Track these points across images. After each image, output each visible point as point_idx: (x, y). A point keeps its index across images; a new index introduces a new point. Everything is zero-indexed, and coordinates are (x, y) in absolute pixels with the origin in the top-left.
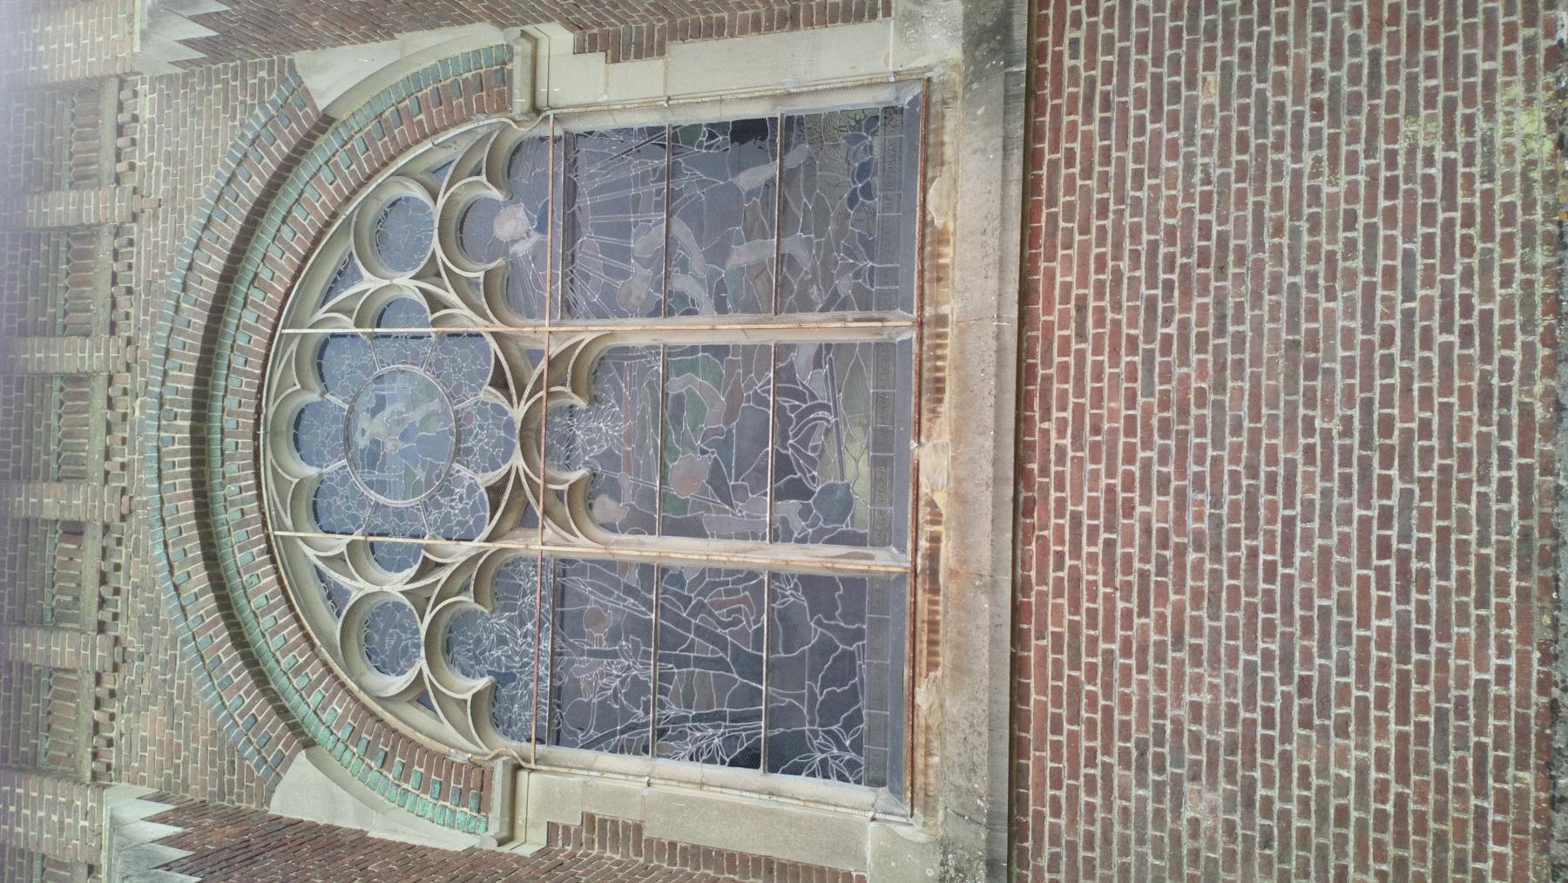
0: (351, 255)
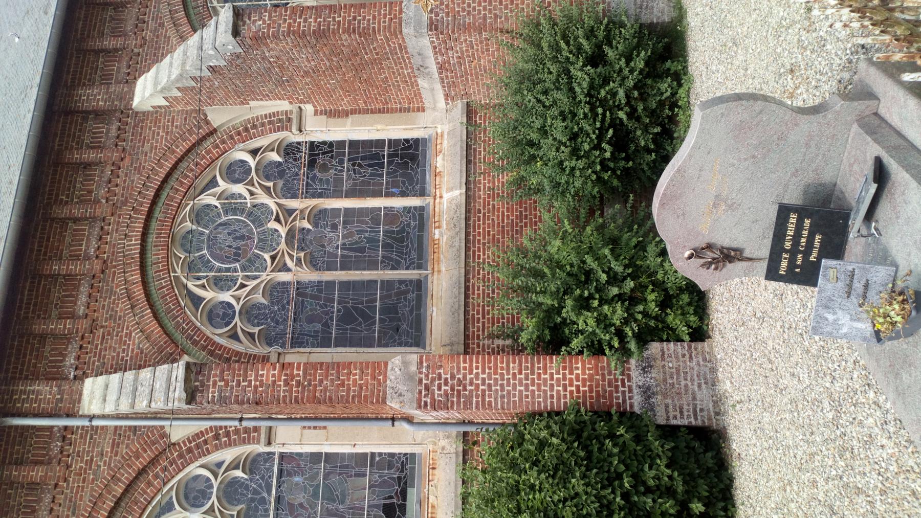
0: (171, 497)
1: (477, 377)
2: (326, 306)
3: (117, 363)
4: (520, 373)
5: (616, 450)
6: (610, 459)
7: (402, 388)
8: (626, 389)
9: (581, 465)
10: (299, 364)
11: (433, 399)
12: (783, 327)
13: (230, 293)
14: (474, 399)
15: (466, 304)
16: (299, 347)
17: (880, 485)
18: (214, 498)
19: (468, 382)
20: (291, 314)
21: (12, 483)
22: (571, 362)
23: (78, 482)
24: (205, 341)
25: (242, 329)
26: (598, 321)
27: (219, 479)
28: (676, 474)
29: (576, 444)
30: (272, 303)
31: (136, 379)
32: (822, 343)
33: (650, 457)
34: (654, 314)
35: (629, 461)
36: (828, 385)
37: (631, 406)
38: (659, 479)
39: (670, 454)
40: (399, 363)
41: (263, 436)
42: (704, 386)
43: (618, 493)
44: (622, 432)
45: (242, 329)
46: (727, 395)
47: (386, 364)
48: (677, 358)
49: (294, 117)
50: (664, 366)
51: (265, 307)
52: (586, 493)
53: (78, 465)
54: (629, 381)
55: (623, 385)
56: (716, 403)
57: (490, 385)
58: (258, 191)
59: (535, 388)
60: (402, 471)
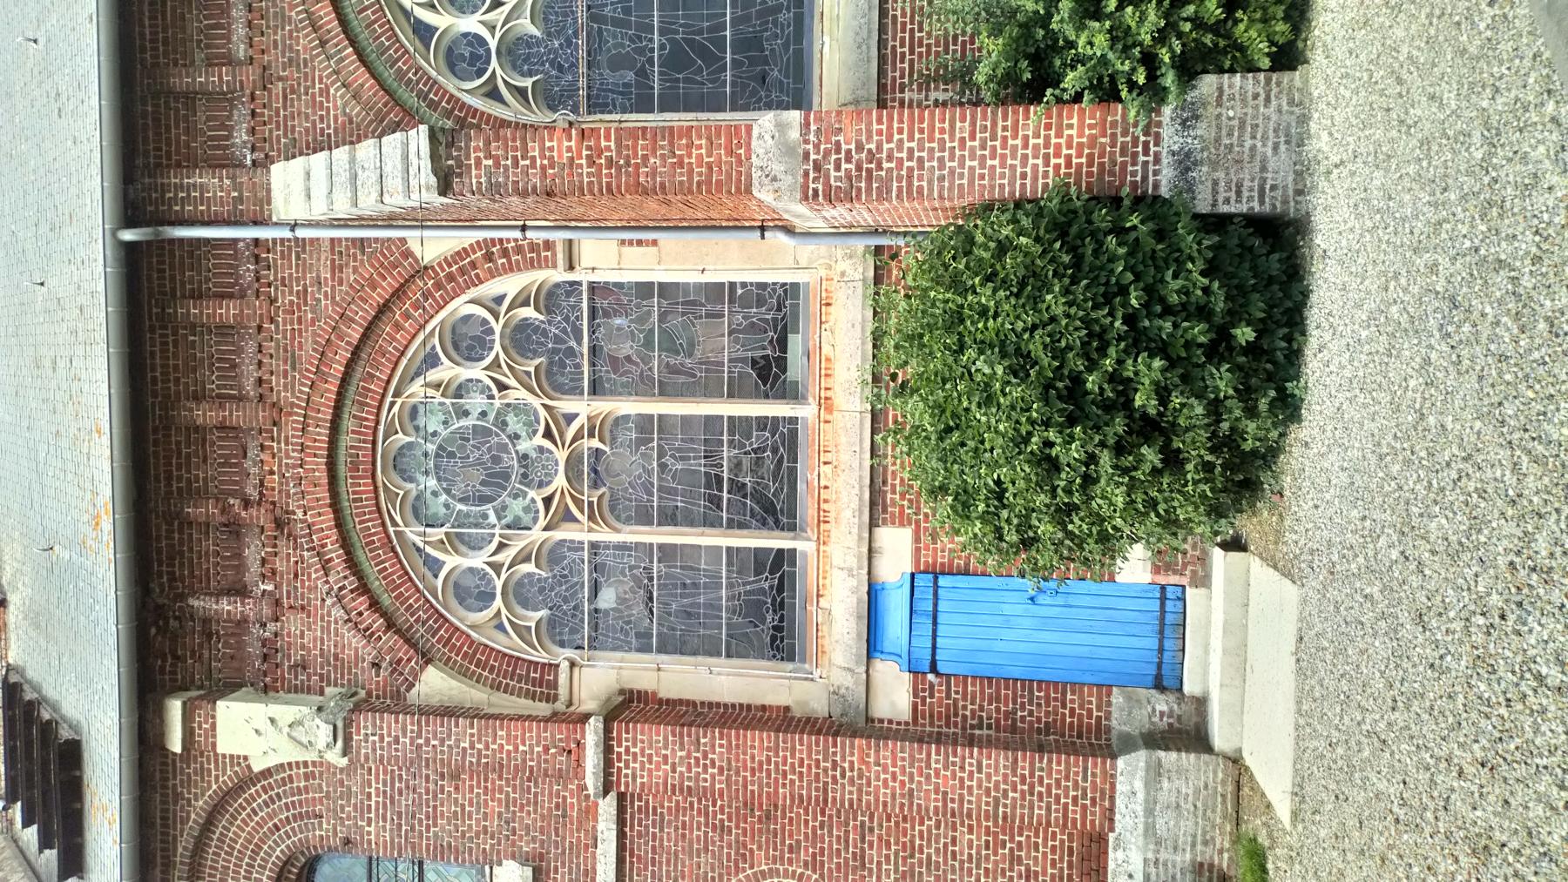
0: (434, 348)
1: (900, 148)
2: (639, 38)
3: (315, 140)
4: (973, 138)
5: (1122, 251)
6: (1111, 266)
7: (777, 168)
8: (1151, 159)
9: (1064, 276)
10: (608, 131)
11: (827, 185)
12: (1430, 16)
13: (478, 16)
14: (895, 184)
15: (882, 29)
16: (602, 112)
17: (1534, 250)
18: (497, 347)
19: (884, 155)
20: (582, 53)
21: (194, 326)
22: (1060, 115)
23: (292, 323)
24: (448, 102)
25: (505, 81)
26: (1114, 40)
27: (502, 321)
28: (1216, 285)
29: (1057, 245)
30: (549, 34)
31: (352, 161)
32: (1489, 33)
33: (1176, 260)
34: (1213, 20)
35: (1141, 267)
36: (1485, 104)
37: (1156, 185)
38: (1187, 294)
39: (1211, 255)
40: (769, 129)
41: (560, 256)
42: (1283, 147)
43: (1120, 314)
44: (1136, 221)
45: (505, 81)
46: (1320, 157)
47: (749, 129)
48: (1244, 101)
50: (1219, 116)
51: (538, 43)
52: (1068, 316)
53: (285, 299)
54: (1156, 145)
55: (1146, 152)
56: (1299, 175)
57: (920, 160)
58: (512, 382)
59: (996, 162)
60: (779, 309)
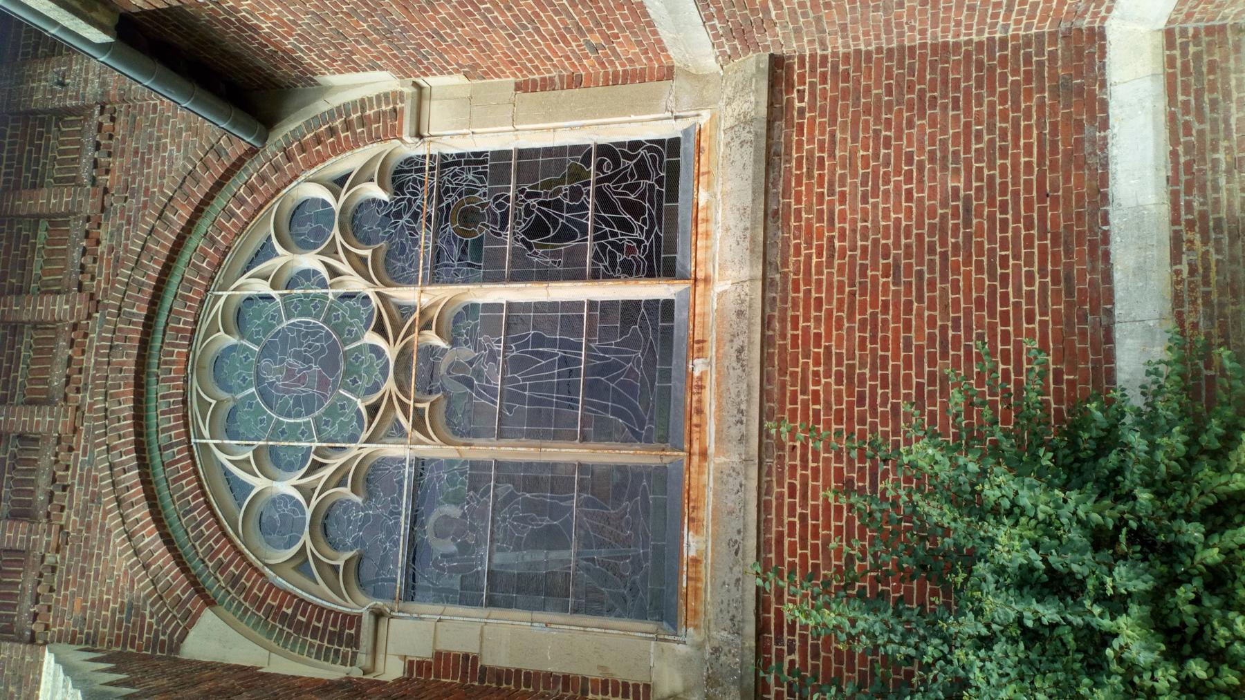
0: (269, 237)
49: (407, 107)
58: (344, 267)
